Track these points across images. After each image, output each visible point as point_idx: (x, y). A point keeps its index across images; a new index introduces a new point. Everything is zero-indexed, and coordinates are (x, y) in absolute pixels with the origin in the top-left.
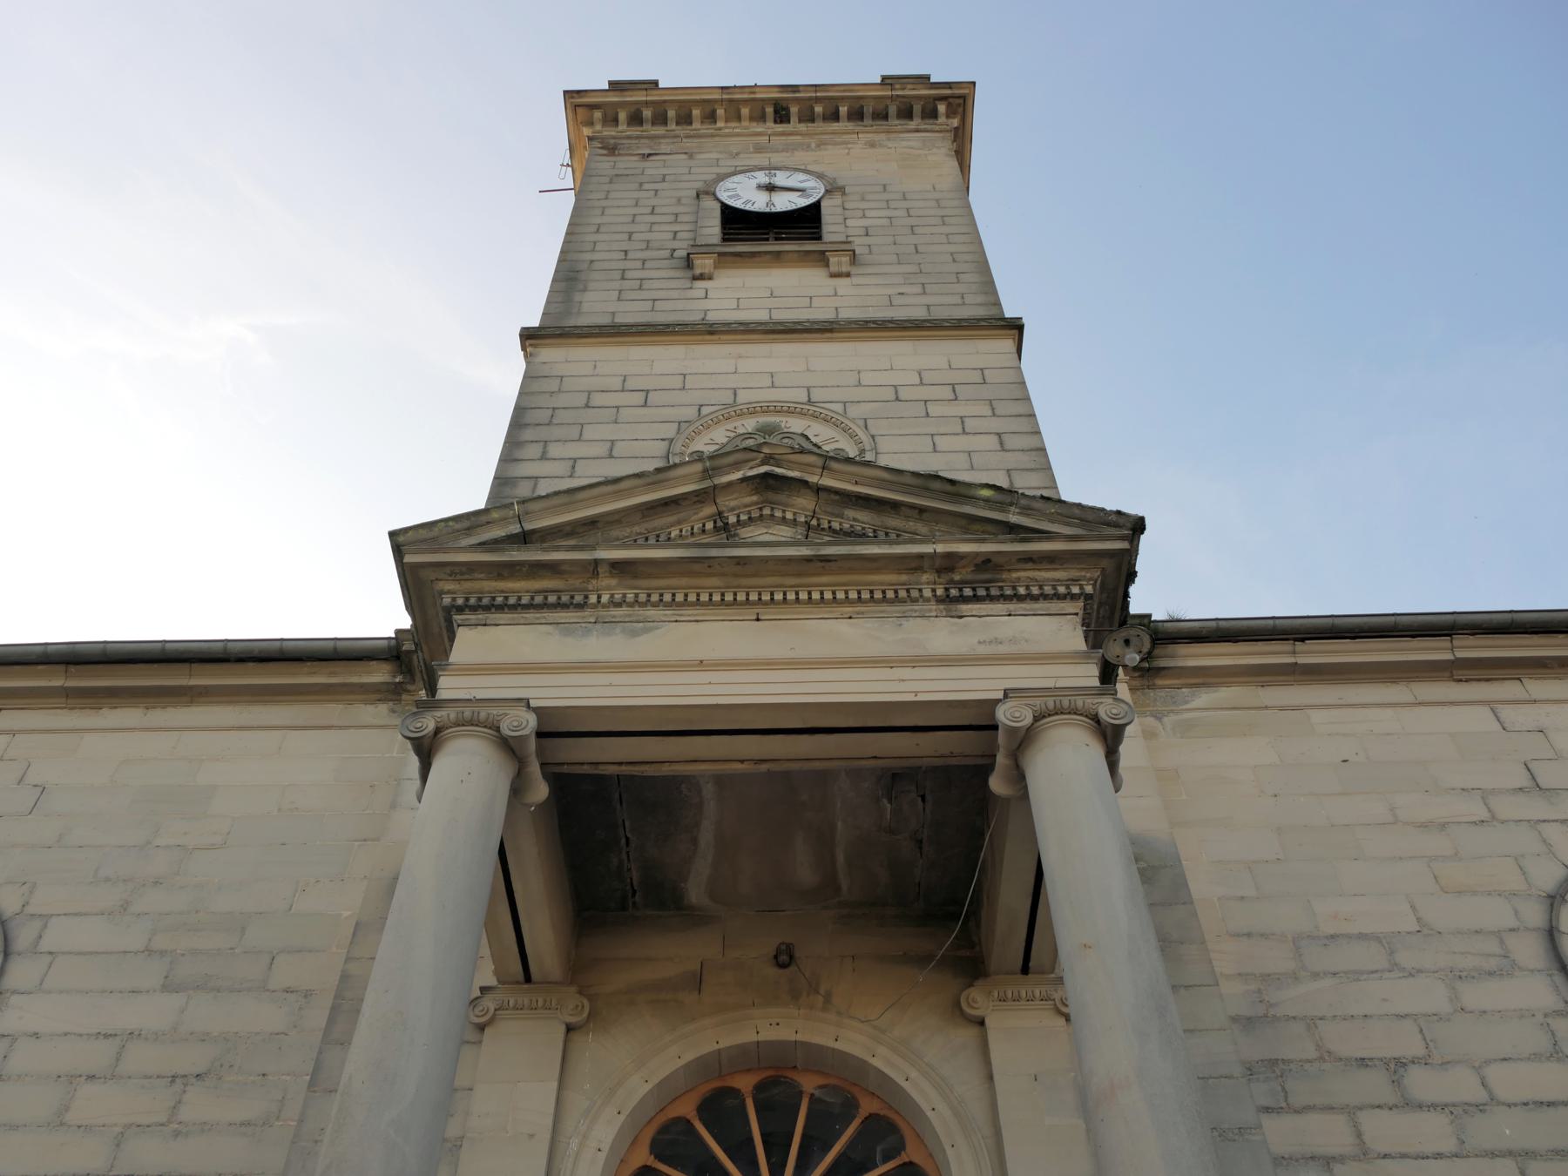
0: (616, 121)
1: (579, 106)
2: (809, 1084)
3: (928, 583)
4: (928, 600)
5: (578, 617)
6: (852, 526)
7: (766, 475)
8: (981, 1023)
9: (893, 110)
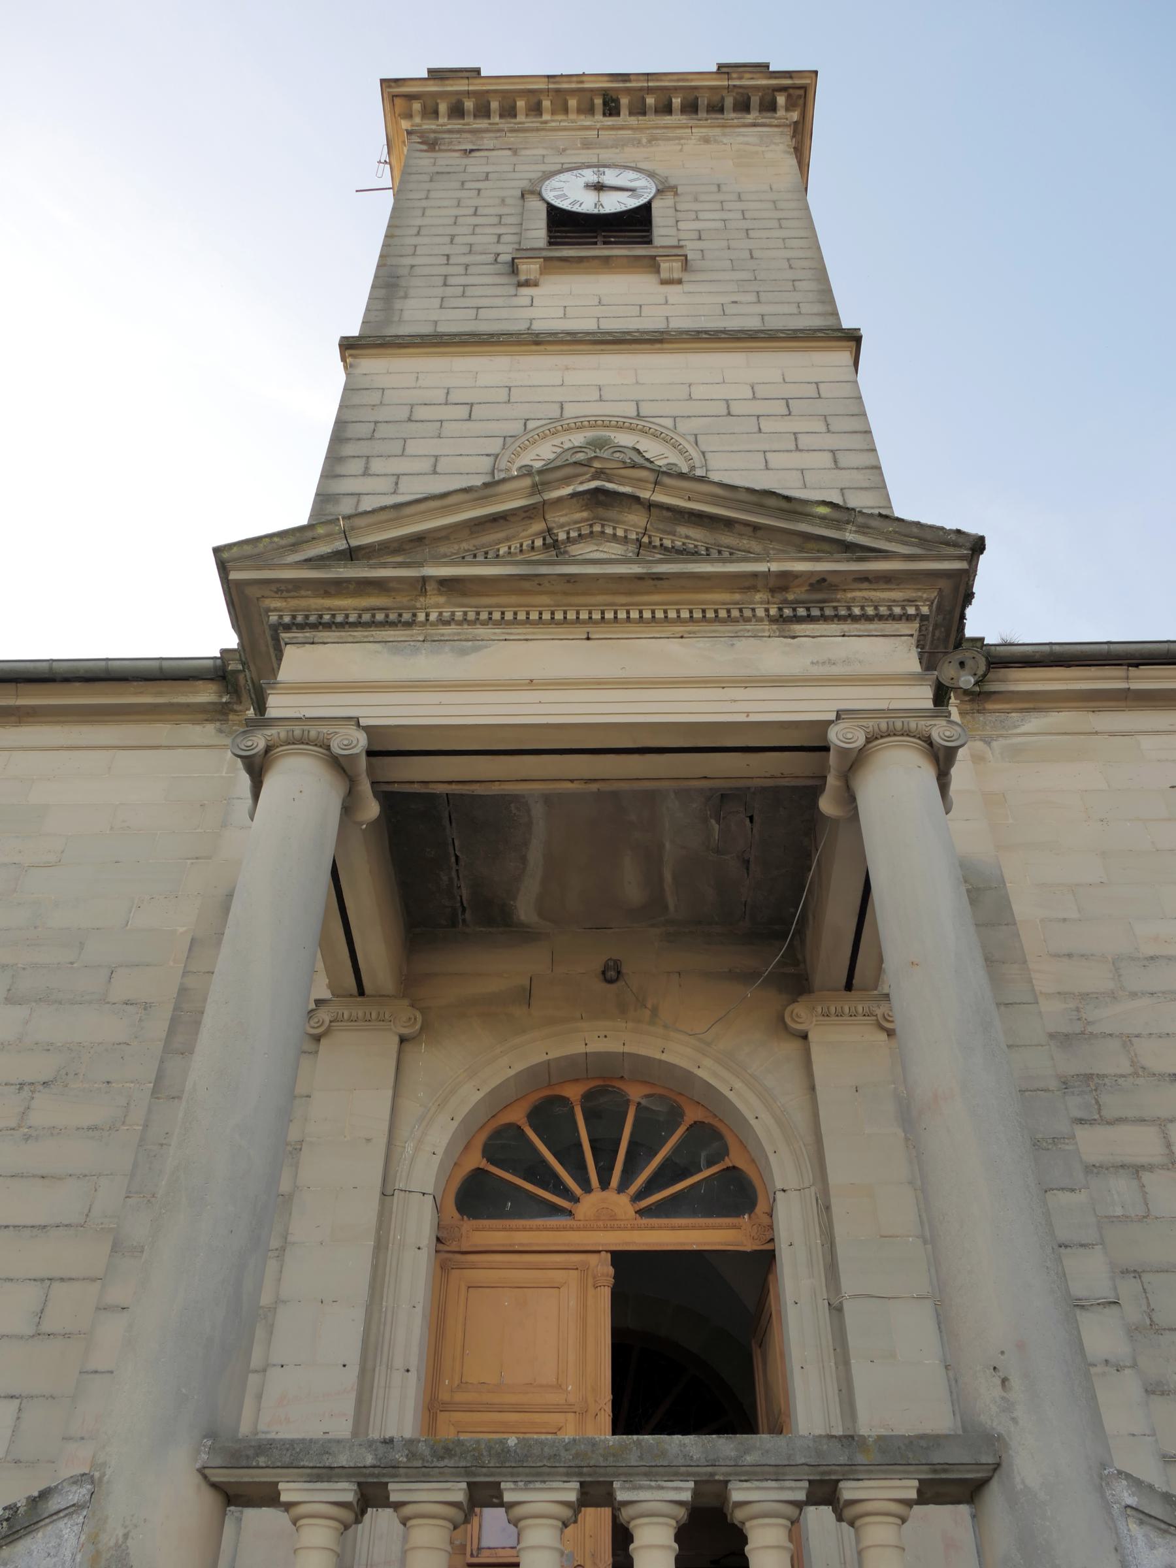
0: (436, 113)
1: (397, 96)
2: (636, 1093)
3: (761, 603)
4: (761, 620)
5: (407, 636)
6: (684, 544)
7: (597, 490)
8: (805, 1037)
9: (729, 102)
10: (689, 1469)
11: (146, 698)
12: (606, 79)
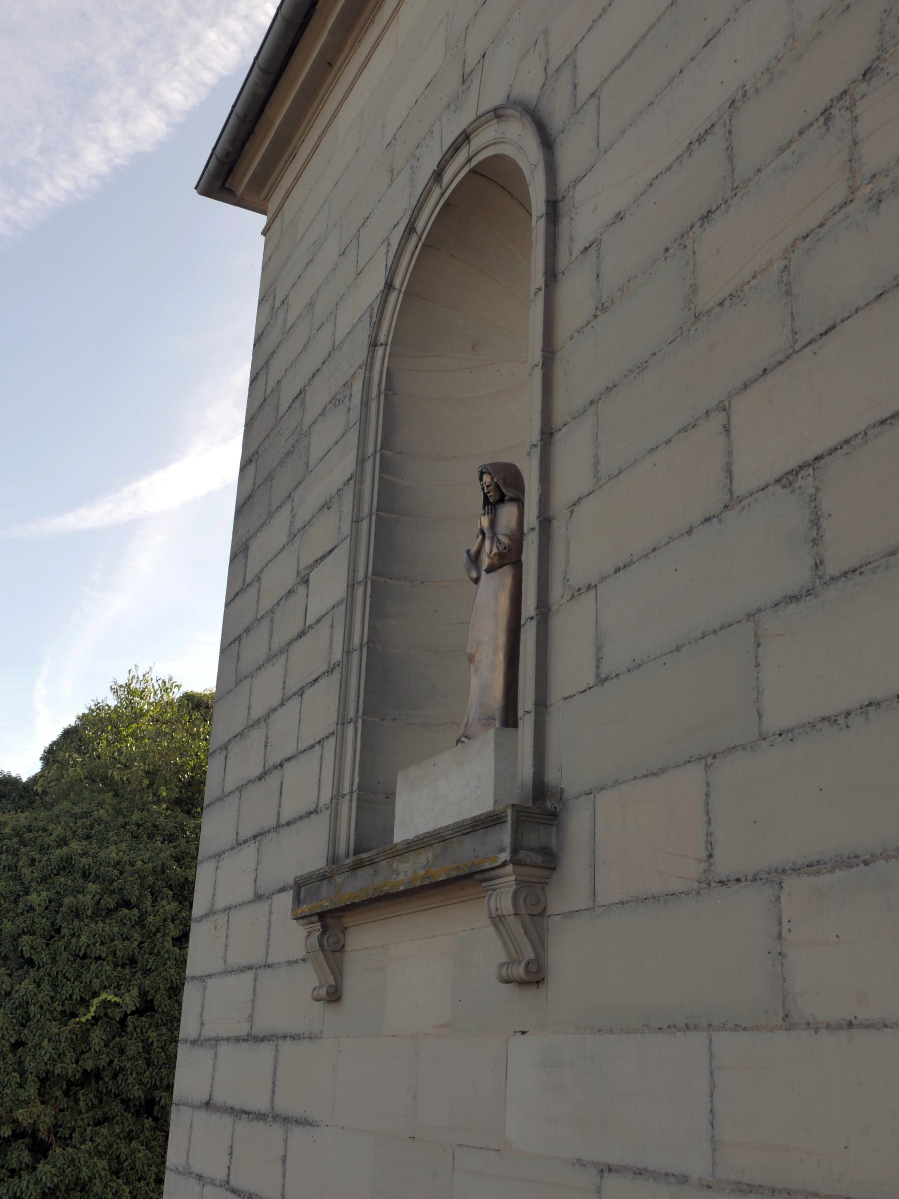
10: (368, 364)
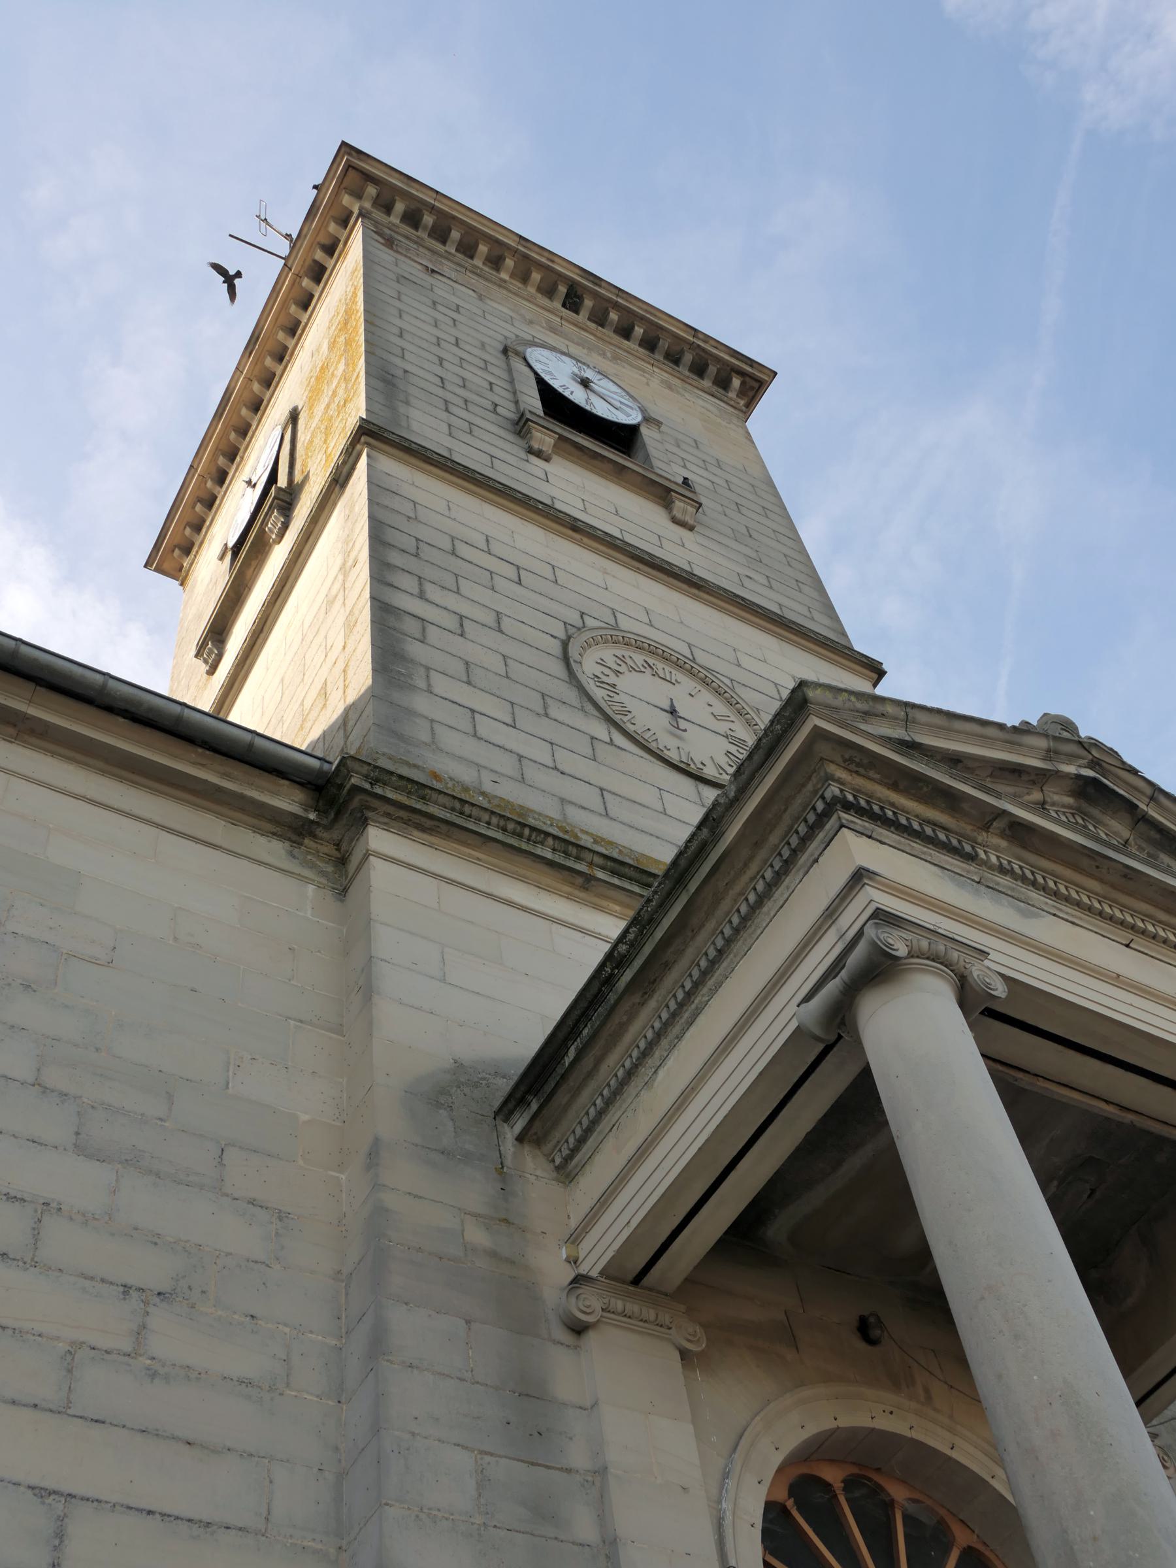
0: (388, 209)
1: (354, 168)
5: (963, 869)
9: (688, 358)
11: (209, 773)
12: (578, 271)
